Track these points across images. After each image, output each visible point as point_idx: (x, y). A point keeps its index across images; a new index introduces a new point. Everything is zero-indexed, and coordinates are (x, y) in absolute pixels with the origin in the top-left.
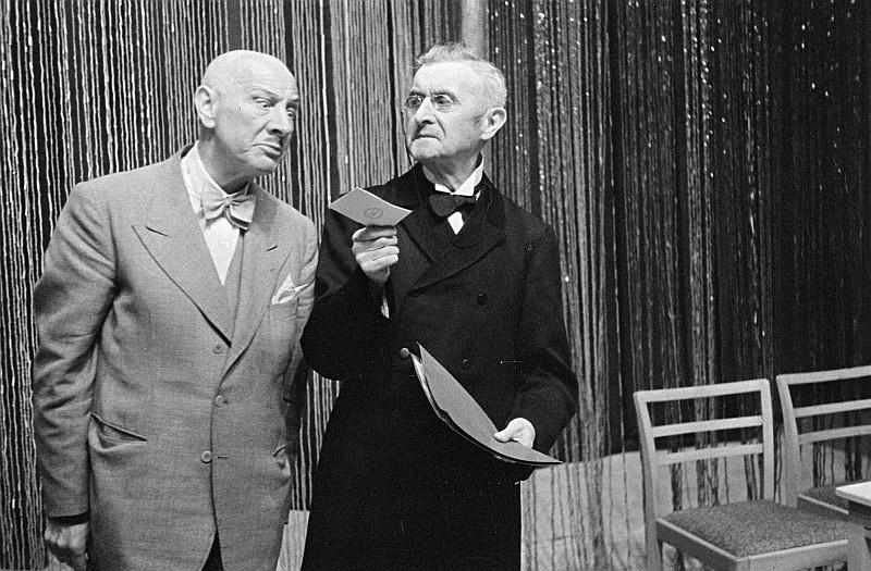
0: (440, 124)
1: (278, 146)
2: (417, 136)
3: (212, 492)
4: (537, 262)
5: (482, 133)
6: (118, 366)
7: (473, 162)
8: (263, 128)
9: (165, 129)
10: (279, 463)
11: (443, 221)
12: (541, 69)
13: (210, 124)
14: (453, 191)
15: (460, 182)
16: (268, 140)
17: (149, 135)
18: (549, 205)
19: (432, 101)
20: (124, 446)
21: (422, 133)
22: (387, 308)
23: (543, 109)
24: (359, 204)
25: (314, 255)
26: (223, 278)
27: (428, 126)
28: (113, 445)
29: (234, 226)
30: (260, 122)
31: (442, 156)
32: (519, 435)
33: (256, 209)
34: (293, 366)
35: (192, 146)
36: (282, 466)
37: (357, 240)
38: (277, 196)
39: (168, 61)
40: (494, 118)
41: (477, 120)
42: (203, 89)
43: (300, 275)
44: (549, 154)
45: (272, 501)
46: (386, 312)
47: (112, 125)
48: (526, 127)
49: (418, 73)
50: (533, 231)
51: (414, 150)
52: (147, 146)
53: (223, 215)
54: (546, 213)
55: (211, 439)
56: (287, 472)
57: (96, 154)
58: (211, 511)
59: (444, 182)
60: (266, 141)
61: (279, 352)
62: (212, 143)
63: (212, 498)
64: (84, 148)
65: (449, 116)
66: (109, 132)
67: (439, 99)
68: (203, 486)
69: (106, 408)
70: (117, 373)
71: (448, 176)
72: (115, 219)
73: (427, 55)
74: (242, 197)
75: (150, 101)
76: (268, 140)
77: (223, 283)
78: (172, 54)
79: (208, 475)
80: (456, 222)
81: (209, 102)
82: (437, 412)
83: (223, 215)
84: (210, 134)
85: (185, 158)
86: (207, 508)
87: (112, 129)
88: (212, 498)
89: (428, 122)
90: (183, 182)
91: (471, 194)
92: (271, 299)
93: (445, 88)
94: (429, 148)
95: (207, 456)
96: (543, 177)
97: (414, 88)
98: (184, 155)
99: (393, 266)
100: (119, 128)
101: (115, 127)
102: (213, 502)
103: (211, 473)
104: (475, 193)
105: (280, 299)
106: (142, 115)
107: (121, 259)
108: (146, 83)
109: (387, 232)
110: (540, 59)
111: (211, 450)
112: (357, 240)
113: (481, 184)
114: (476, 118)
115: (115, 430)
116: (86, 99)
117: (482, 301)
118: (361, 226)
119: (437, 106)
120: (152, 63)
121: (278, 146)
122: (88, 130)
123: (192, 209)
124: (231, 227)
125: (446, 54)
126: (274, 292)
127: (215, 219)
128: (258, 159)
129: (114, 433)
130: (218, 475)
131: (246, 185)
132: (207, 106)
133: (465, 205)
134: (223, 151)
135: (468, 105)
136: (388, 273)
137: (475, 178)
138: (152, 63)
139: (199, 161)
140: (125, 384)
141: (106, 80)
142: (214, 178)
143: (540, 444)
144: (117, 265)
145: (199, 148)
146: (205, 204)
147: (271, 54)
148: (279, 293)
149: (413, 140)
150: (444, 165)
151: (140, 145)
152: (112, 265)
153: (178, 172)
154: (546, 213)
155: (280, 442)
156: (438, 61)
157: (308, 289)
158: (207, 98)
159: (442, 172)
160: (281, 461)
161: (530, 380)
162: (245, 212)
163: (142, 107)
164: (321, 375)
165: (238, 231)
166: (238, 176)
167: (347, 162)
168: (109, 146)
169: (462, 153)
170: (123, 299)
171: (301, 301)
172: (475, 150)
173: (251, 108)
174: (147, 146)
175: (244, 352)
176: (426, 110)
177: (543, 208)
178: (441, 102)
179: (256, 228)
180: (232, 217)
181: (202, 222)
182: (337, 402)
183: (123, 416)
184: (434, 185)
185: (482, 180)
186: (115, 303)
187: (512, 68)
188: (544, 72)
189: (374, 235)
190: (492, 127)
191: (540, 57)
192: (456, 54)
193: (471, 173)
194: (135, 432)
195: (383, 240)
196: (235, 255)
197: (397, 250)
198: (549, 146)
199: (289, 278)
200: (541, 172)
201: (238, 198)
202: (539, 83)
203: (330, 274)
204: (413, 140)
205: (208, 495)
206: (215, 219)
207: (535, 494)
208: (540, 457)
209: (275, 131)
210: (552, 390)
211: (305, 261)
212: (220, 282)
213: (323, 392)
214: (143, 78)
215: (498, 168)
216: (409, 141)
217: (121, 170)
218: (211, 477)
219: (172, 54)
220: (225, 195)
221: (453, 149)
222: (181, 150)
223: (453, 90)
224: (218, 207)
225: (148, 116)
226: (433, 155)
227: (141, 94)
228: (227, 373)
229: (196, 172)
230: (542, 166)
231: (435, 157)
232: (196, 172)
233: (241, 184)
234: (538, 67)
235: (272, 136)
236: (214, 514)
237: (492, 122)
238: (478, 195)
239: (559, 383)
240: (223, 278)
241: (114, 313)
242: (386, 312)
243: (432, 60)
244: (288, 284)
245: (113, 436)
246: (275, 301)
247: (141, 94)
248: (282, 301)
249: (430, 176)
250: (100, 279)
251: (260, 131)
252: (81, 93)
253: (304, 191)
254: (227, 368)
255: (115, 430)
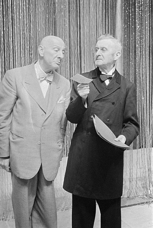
0: (103, 57)
1: (60, 62)
2: (97, 59)
3: (40, 152)
4: (130, 93)
5: (114, 58)
6: (17, 118)
7: (112, 66)
8: (56, 57)
9: (33, 55)
10: (59, 145)
11: (103, 82)
12: (138, 41)
13: (42, 55)
14: (107, 74)
15: (109, 72)
16: (58, 60)
17: (32, 58)
18: (139, 78)
19: (101, 50)
20: (18, 139)
21: (98, 58)
22: (87, 105)
23: (138, 52)
24: (79, 78)
25: (69, 90)
26: (45, 95)
27: (99, 56)
28: (15, 139)
29: (48, 82)
30: (55, 55)
31: (103, 65)
32: (120, 141)
33: (54, 78)
34: (63, 119)
35: (37, 61)
36: (60, 146)
37: (78, 87)
38: (60, 74)
39: (38, 38)
40: (118, 54)
41: (113, 55)
42: (40, 46)
43: (65, 95)
44: (139, 64)
45: (57, 155)
46: (86, 106)
47: (23, 55)
48: (133, 57)
49: (97, 42)
50: (128, 85)
51: (96, 63)
52: (32, 61)
53: (45, 79)
54: (138, 80)
55: (40, 139)
56: (61, 147)
57: (19, 62)
58: (40, 157)
59: (104, 71)
60: (57, 61)
61: (59, 117)
62: (43, 60)
63: (40, 154)
64: (16, 61)
65: (106, 54)
66: (22, 57)
67: (102, 49)
68: (38, 150)
69: (14, 129)
70: (17, 121)
71: (105, 70)
72: (17, 79)
73: (100, 38)
74: (50, 75)
75: (33, 49)
76: (58, 60)
77: (44, 98)
78: (39, 36)
79: (39, 148)
80: (107, 82)
81: (42, 49)
82: (97, 133)
83: (45, 79)
84: (42, 58)
85: (35, 64)
86: (39, 156)
87: (23, 56)
88: (40, 154)
89: (99, 55)
90: (35, 71)
91: (111, 74)
92: (57, 101)
93: (104, 46)
94: (100, 63)
95: (39, 143)
96: (137, 70)
97: (96, 46)
98: (35, 63)
99: (88, 94)
100: (25, 56)
101: (24, 55)
102: (41, 155)
103: (40, 147)
104: (113, 74)
105: (60, 101)
106: (31, 52)
107: (18, 90)
108: (32, 44)
109: (86, 85)
110: (138, 38)
111: (40, 141)
112: (78, 87)
113: (115, 72)
114: (113, 54)
115: (16, 135)
116: (16, 48)
117: (113, 103)
118: (80, 84)
119: (102, 51)
120: (34, 39)
121: (60, 62)
122: (17, 56)
123: (37, 78)
124: (47, 82)
125: (105, 37)
126: (58, 100)
127: (43, 80)
128: (55, 65)
129: (16, 136)
130: (42, 148)
131: (51, 71)
132: (41, 51)
133: (110, 78)
134: (45, 62)
135: (110, 51)
136: (87, 96)
137: (113, 70)
138: (34, 39)
139: (39, 65)
140: (19, 123)
141: (22, 43)
142: (43, 70)
143: (128, 143)
144: (17, 92)
145: (39, 61)
146: (40, 76)
147: (60, 37)
148: (59, 100)
149: (96, 60)
150: (104, 67)
151: (30, 60)
152: (16, 92)
153: (34, 68)
154: (138, 80)
155: (59, 139)
156: (103, 39)
157: (68, 99)
158: (42, 49)
159: (104, 69)
160: (60, 145)
161: (126, 125)
162: (51, 79)
163: (31, 50)
164: (71, 122)
165: (49, 84)
166: (49, 69)
167: (84, 65)
168: (22, 60)
169: (109, 64)
170: (18, 101)
171: (66, 102)
172: (113, 63)
173: (53, 52)
174: (32, 61)
175: (49, 116)
176: (99, 52)
177: (137, 79)
178: (103, 50)
179: (54, 83)
180: (48, 80)
181: (39, 81)
182: (76, 129)
183: (18, 132)
184: (101, 72)
185: (115, 71)
186: (17, 102)
187: (130, 41)
188: (139, 42)
189: (83, 86)
190: (117, 57)
191: (137, 38)
192: (107, 37)
193: (112, 69)
194: (21, 136)
195: (85, 87)
196: (48, 90)
197: (89, 90)
198: (139, 62)
199: (62, 96)
200: (137, 69)
201: (49, 75)
202: (137, 45)
203: (74, 96)
204: (96, 60)
205: (39, 153)
206: (43, 80)
207: (132, 156)
208: (126, 146)
209: (59, 58)
210: (132, 128)
211: (67, 91)
212: (44, 97)
213: (72, 127)
214: (31, 43)
215: (125, 68)
216: (95, 60)
217: (25, 65)
218: (40, 148)
219: (39, 36)
220: (46, 74)
221: (106, 63)
222: (34, 62)
223: (107, 47)
224: (44, 77)
225: (32, 53)
226: (100, 64)
227: (30, 47)
228: (45, 121)
229: (38, 69)
230: (137, 68)
231: (101, 65)
232: (38, 69)
233: (50, 72)
234: (137, 41)
235: (59, 59)
236: (41, 158)
237: (117, 55)
238: (113, 75)
239: (133, 125)
240: (45, 95)
241: (16, 105)
242: (86, 106)
243: (101, 39)
244: (62, 98)
245: (15, 137)
246: (58, 102)
247: (30, 47)
248: (60, 102)
249: (100, 70)
250: (14, 97)
251: (55, 58)
252: (15, 47)
253: (72, 74)
254: (45, 120)
255: (16, 135)
